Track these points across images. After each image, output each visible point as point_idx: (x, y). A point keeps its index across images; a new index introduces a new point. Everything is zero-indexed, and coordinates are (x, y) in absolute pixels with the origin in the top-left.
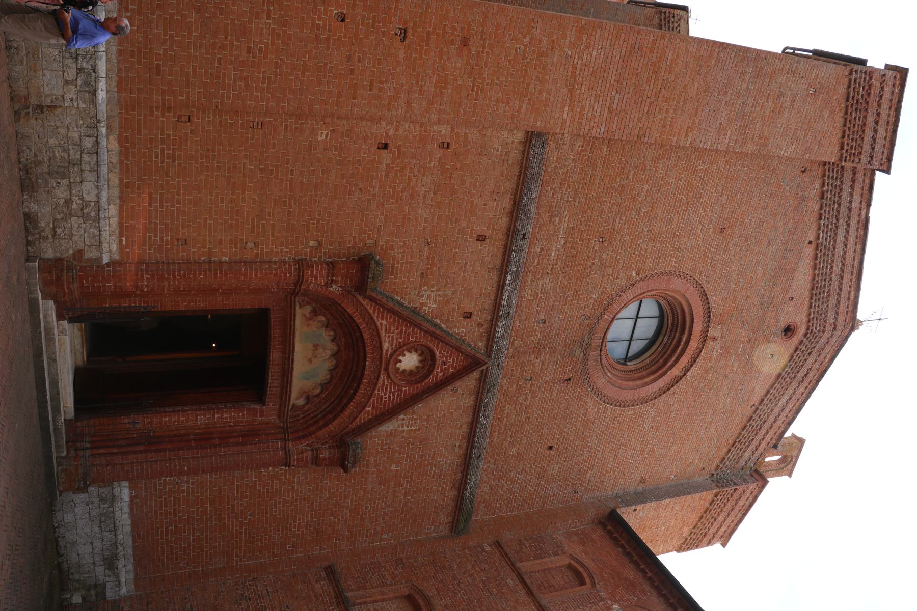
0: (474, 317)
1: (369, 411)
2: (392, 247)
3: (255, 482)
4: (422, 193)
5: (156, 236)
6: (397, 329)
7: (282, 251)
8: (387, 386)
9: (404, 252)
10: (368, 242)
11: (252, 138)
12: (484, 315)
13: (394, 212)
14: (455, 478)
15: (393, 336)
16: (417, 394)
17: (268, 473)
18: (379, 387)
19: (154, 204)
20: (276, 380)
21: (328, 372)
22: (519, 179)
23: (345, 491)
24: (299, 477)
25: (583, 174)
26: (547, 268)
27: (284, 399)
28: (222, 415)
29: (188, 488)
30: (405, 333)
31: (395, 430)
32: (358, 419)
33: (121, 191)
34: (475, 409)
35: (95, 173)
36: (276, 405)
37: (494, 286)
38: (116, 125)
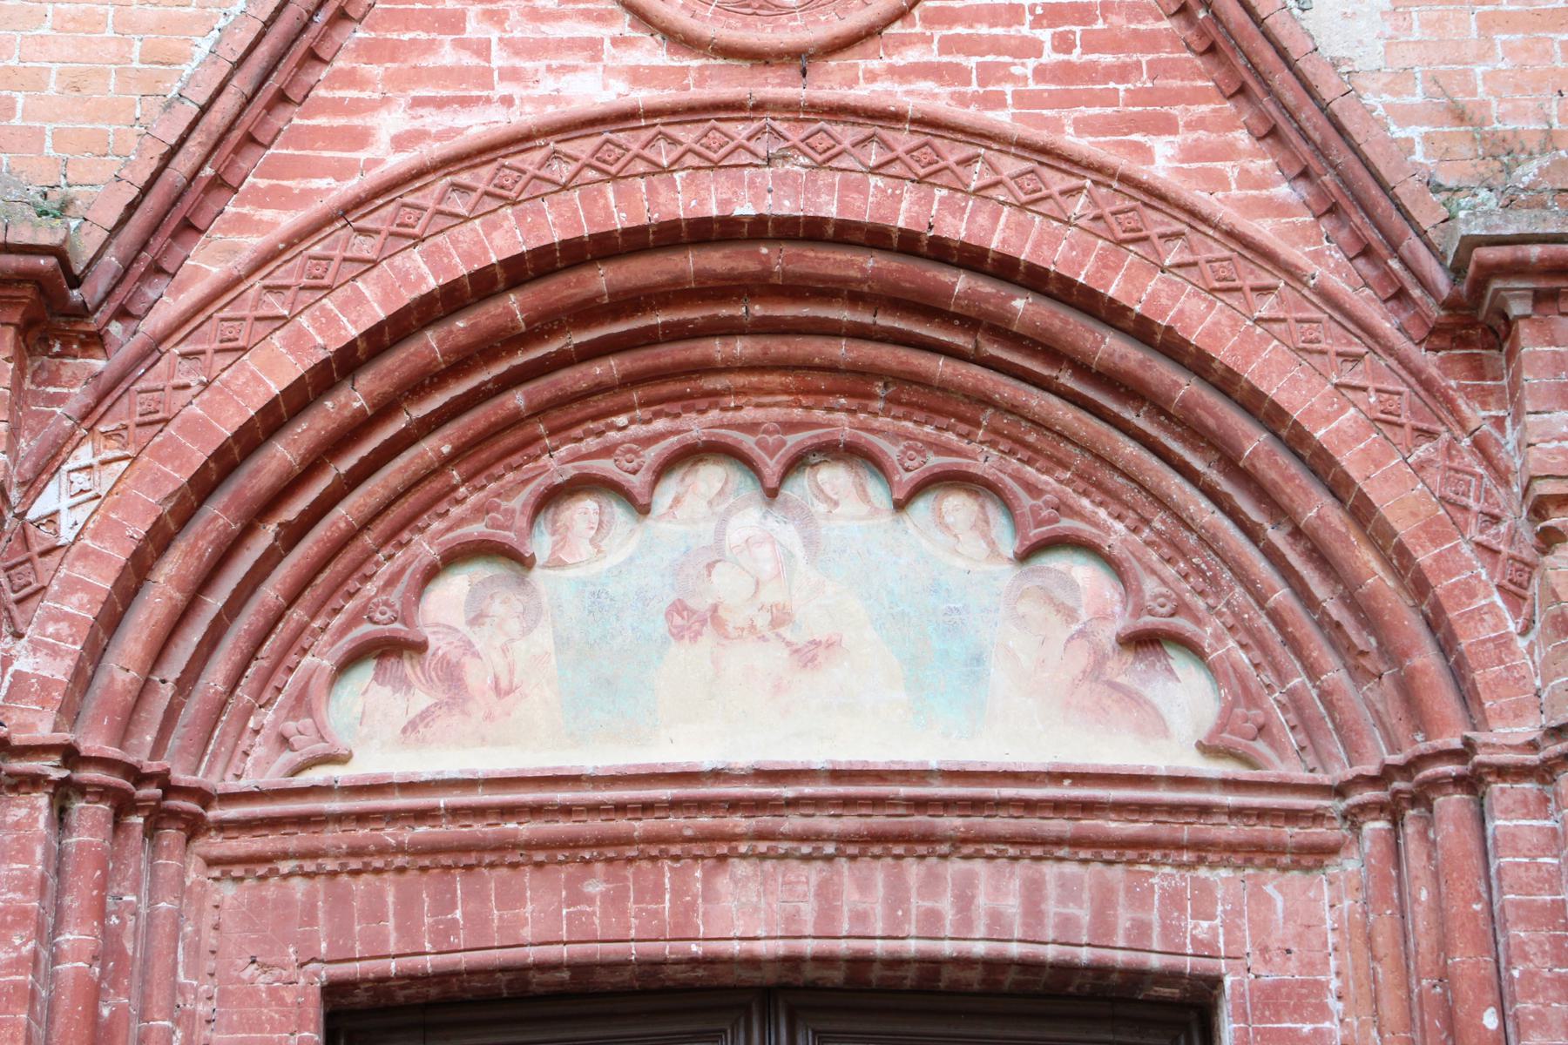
1: (1190, 153)
8: (947, 45)
15: (514, 47)
18: (963, 100)
20: (964, 902)
21: (922, 508)
32: (1263, 229)
36: (1205, 888)
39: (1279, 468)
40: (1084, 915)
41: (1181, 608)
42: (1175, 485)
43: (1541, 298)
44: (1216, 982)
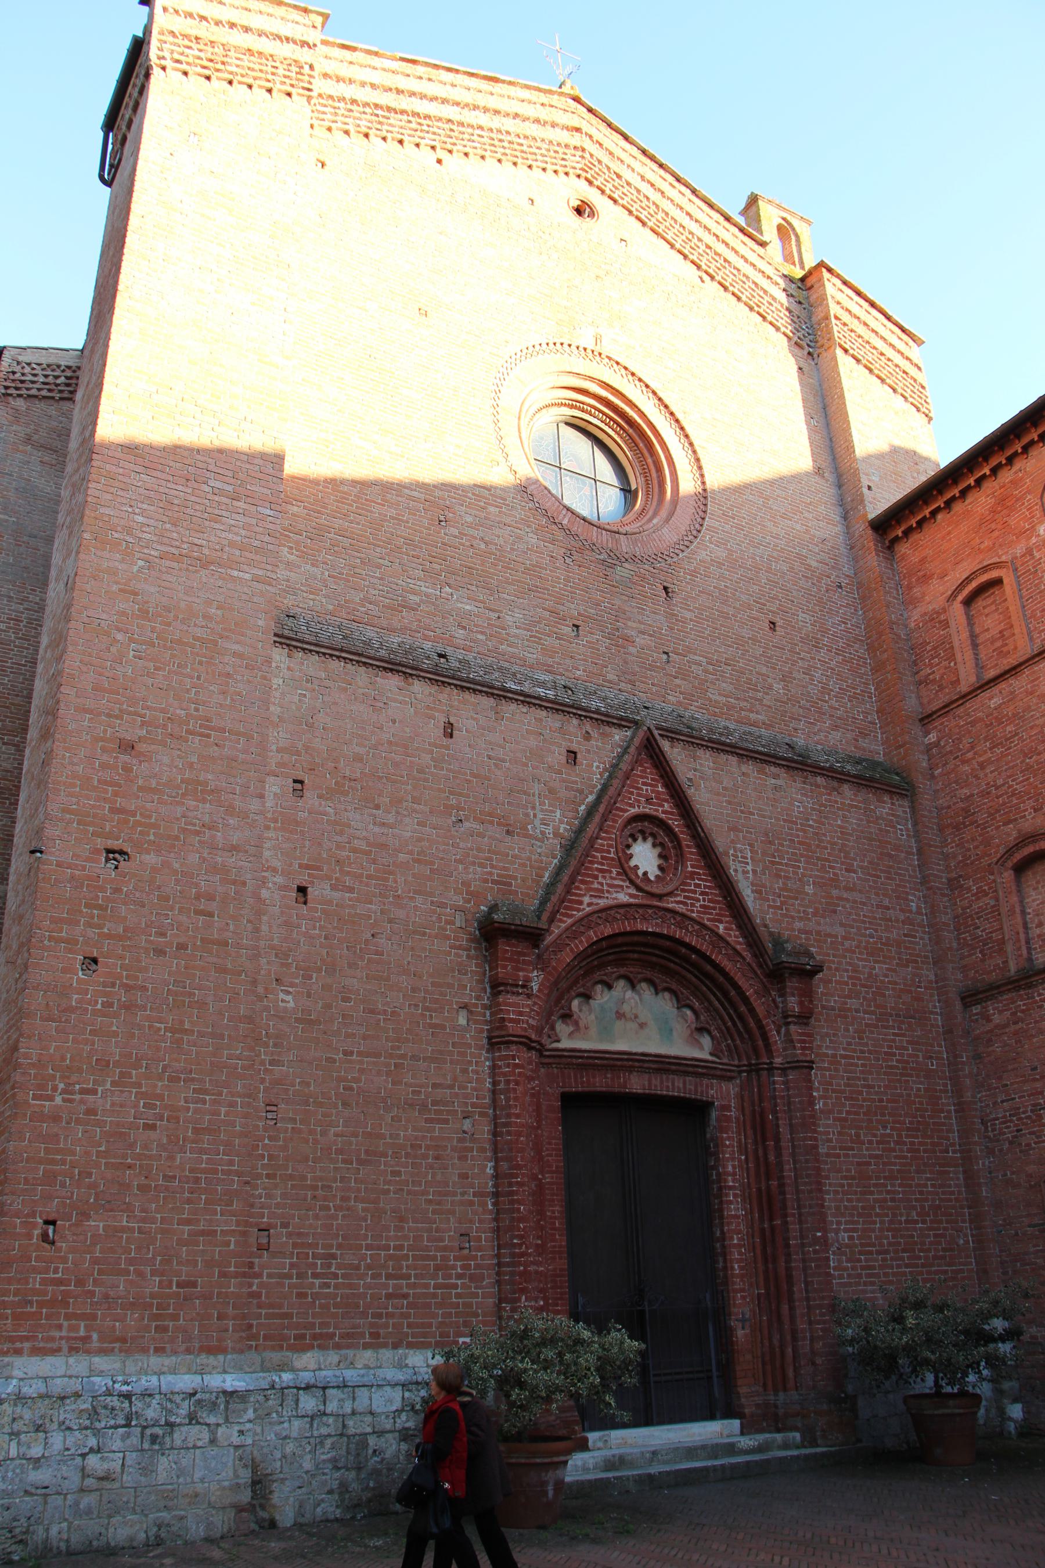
0: (574, 747)
1: (725, 928)
2: (466, 884)
3: (835, 1119)
4: (377, 829)
5: (455, 1286)
6: (596, 877)
7: (476, 1072)
8: (685, 897)
9: (474, 864)
10: (458, 924)
11: (294, 1120)
12: (571, 729)
13: (410, 878)
14: (825, 787)
15: (609, 885)
16: (698, 846)
17: (821, 1097)
18: (688, 910)
19: (405, 1290)
20: (673, 1084)
21: (660, 995)
22: (351, 660)
23: (847, 971)
24: (827, 1047)
25: (336, 548)
26: (490, 619)
27: (704, 1071)
28: (728, 1174)
29: (846, 1230)
30: (603, 864)
31: (752, 884)
32: (738, 947)
33: (385, 1346)
34: (717, 749)
35: (356, 1389)
37: (525, 710)
38: (276, 1356)
39: (737, 999)
40: (693, 1088)
41: (708, 1023)
42: (712, 998)
43: (791, 974)
44: (713, 1103)
